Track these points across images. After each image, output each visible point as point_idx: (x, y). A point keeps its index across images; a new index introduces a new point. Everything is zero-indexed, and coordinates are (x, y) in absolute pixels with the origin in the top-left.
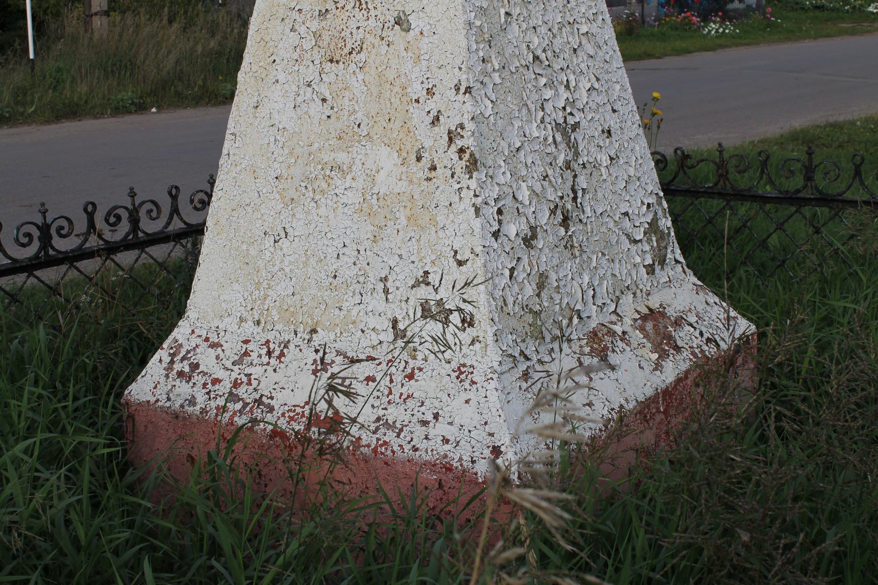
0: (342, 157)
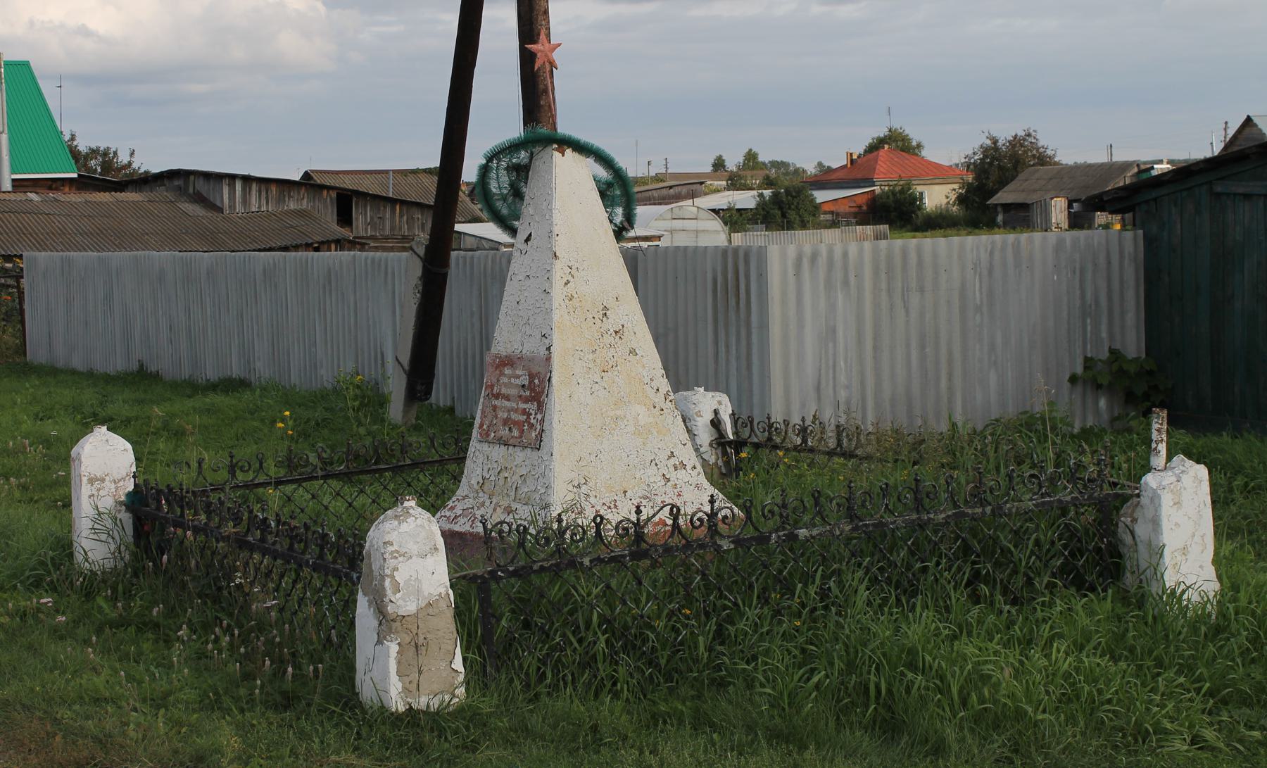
0: (618, 412)
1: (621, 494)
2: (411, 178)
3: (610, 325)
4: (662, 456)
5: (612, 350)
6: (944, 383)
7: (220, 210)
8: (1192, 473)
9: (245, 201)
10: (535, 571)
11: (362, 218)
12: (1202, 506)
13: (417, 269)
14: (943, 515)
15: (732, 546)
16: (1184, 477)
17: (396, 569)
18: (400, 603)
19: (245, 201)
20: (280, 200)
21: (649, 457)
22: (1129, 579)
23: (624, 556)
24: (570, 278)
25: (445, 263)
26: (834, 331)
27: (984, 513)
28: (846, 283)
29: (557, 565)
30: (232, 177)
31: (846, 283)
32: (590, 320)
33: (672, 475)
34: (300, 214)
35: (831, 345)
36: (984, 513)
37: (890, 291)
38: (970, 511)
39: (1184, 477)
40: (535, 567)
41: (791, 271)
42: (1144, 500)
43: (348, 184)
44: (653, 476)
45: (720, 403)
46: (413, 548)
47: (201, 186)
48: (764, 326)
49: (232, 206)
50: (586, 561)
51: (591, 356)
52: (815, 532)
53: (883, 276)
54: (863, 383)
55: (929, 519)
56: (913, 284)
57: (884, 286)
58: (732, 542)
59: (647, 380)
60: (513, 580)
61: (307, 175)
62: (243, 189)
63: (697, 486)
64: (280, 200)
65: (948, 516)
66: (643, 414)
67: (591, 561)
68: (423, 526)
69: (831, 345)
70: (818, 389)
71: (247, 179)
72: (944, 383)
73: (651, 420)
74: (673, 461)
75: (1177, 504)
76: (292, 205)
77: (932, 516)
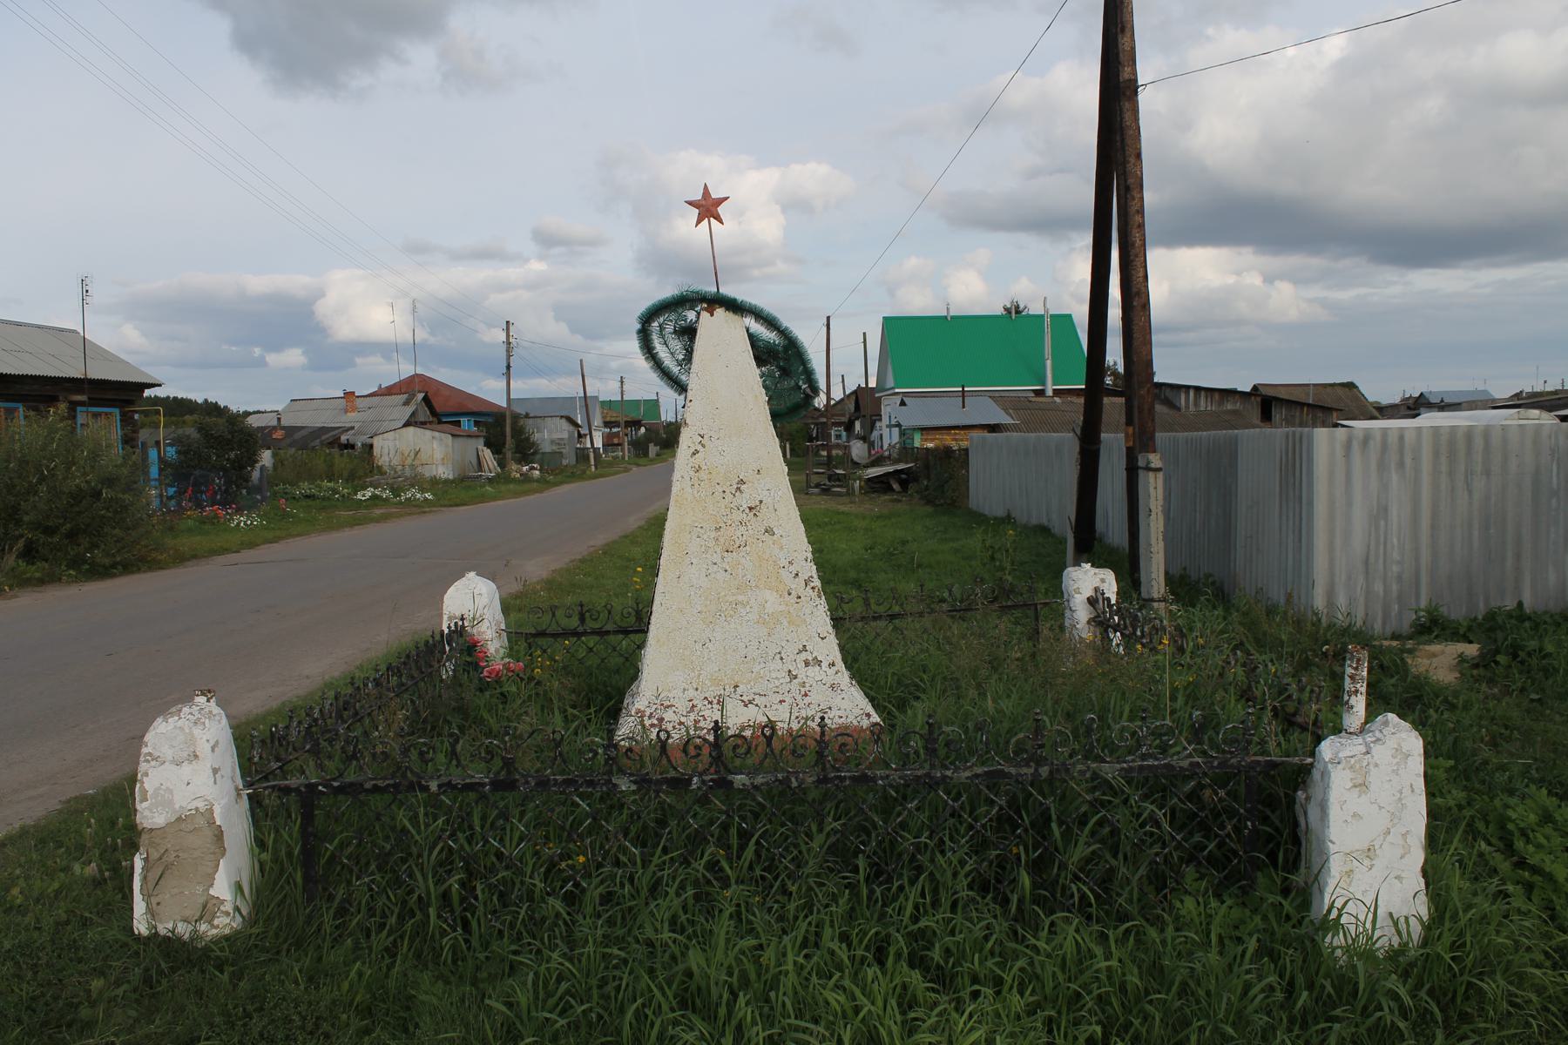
0: (740, 598)
1: (729, 689)
2: (1329, 390)
3: (745, 501)
4: (790, 650)
5: (742, 529)
6: (1509, 563)
7: (1179, 409)
8: (1391, 743)
9: (1196, 404)
10: (367, 791)
11: (1278, 414)
12: (1407, 791)
13: (1075, 447)
14: (968, 774)
15: (634, 787)
16: (1376, 749)
17: (146, 775)
18: (147, 813)
19: (1196, 404)
20: (1221, 403)
21: (773, 650)
22: (1298, 879)
23: (483, 785)
24: (699, 447)
25: (1097, 441)
26: (1386, 510)
27: (1036, 774)
28: (1401, 464)
29: (396, 786)
30: (1188, 387)
31: (1401, 464)
32: (718, 495)
33: (801, 671)
34: (1235, 412)
35: (1382, 523)
36: (1036, 774)
37: (1451, 474)
38: (1013, 771)
39: (1376, 749)
40: (368, 786)
41: (1340, 452)
42: (1316, 774)
43: (1271, 393)
44: (777, 670)
45: (1103, 581)
46: (167, 752)
47: (1168, 392)
48: (1310, 503)
49: (1187, 406)
50: (434, 786)
51: (713, 534)
52: (759, 780)
53: (1444, 460)
54: (1417, 559)
55: (944, 777)
56: (1479, 468)
57: (1444, 468)
58: (635, 782)
59: (784, 562)
60: (341, 797)
61: (1255, 388)
62: (538, 372)
63: (832, 687)
64: (1221, 403)
65: (977, 776)
66: (773, 601)
67: (440, 786)
68: (181, 728)
69: (1382, 523)
70: (1366, 562)
71: (1198, 389)
72: (1509, 563)
73: (782, 608)
74: (804, 656)
75: (1362, 786)
76: (1229, 407)
77: (949, 773)
